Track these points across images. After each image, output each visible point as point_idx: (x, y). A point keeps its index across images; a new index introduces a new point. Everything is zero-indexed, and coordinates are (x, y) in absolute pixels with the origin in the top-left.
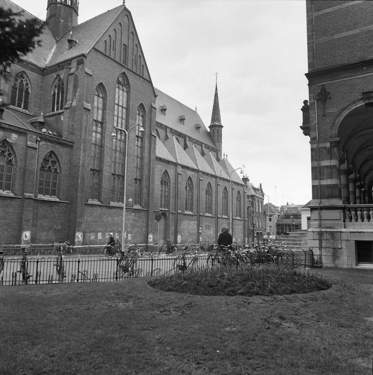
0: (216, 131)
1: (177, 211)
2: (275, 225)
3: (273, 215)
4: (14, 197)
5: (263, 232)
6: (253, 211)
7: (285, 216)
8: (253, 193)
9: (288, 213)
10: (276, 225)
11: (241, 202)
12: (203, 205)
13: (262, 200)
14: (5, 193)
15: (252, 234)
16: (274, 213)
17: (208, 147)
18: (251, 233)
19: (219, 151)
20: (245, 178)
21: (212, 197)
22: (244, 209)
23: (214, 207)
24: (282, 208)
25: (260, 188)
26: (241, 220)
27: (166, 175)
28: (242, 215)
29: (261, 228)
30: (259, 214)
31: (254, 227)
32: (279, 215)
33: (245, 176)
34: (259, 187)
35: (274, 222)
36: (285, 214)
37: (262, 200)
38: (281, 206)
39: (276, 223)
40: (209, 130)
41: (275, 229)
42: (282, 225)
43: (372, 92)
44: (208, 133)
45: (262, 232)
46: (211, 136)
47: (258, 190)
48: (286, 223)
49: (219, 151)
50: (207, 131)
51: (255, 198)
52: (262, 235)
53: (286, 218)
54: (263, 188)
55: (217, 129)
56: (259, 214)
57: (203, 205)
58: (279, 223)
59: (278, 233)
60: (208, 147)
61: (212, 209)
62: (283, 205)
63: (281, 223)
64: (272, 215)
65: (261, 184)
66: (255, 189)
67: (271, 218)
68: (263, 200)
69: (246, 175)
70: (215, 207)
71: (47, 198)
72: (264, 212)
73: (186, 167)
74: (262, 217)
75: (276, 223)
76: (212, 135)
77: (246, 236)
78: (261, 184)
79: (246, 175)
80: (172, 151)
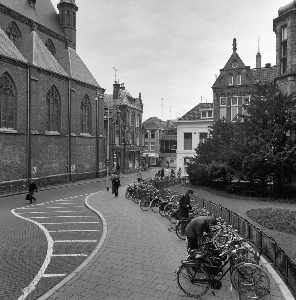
0: (66, 12)
1: (98, 135)
2: (158, 142)
3: (157, 130)
4: (17, 133)
5: (141, 150)
6: (124, 125)
7: (170, 131)
8: (126, 102)
9: (173, 127)
10: (160, 141)
11: (91, 111)
12: (76, 122)
13: (140, 113)
14: (3, 129)
15: (122, 154)
16: (157, 128)
17: (57, 36)
18: (121, 153)
19: (71, 41)
20: (116, 85)
21: (16, 99)
22: (97, 121)
23: (63, 121)
24: (168, 121)
25: (139, 99)
26: (92, 138)
27: (86, 100)
28: (93, 130)
29: (138, 145)
30: (135, 129)
31: (125, 145)
32: (164, 131)
33: (117, 81)
34: (138, 98)
35: (157, 138)
36: (170, 129)
37: (140, 113)
38: (167, 120)
39: (160, 139)
40: (58, 12)
41: (158, 146)
42: (167, 142)
43: (270, 299)
44: (57, 16)
45: (139, 150)
46: (59, 19)
47: (134, 100)
48: (170, 139)
49: (71, 41)
50: (56, 13)
51: (127, 108)
52: (140, 154)
53: (171, 134)
54: (142, 98)
55: (67, 10)
56: (135, 129)
57: (76, 122)
58: (163, 139)
59: (162, 151)
60: (57, 36)
61: (16, 121)
62: (169, 119)
63: (165, 139)
64: (155, 130)
65: (140, 94)
66: (130, 99)
67: (154, 134)
68: (142, 112)
69: (119, 80)
70: (26, 117)
71: (51, 133)
72: (143, 127)
73: (81, 82)
74: (140, 133)
75: (160, 139)
76: (61, 19)
77: (100, 159)
78: (140, 94)
79: (119, 80)
80: (27, 51)
